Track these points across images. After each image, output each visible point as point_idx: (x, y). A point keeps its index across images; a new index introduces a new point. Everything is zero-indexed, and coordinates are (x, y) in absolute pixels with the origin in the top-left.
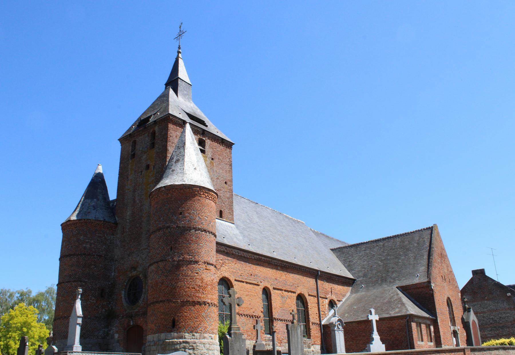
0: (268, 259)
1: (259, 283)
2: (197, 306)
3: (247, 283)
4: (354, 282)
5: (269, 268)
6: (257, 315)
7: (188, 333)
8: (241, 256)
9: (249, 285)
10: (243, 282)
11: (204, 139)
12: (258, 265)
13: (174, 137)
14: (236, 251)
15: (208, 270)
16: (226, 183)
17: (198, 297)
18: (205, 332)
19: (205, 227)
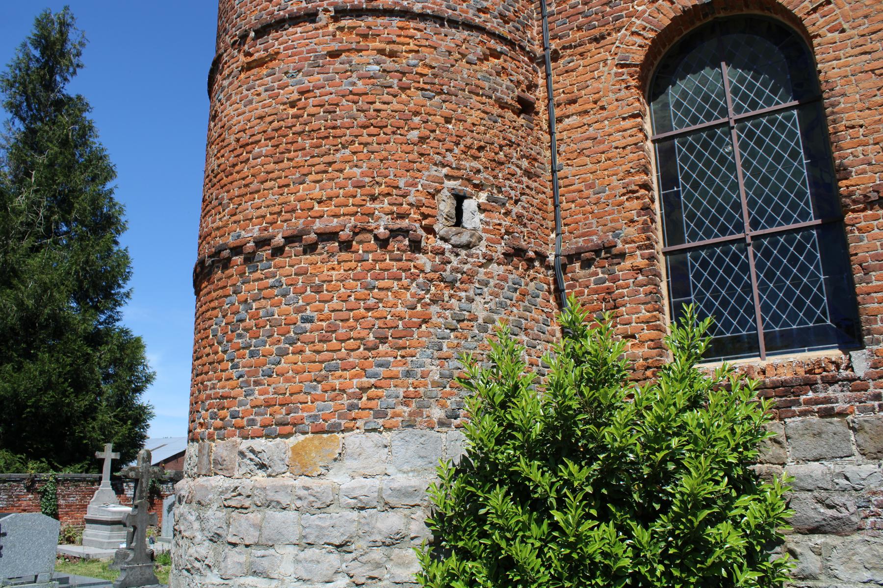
15: (261, 63)
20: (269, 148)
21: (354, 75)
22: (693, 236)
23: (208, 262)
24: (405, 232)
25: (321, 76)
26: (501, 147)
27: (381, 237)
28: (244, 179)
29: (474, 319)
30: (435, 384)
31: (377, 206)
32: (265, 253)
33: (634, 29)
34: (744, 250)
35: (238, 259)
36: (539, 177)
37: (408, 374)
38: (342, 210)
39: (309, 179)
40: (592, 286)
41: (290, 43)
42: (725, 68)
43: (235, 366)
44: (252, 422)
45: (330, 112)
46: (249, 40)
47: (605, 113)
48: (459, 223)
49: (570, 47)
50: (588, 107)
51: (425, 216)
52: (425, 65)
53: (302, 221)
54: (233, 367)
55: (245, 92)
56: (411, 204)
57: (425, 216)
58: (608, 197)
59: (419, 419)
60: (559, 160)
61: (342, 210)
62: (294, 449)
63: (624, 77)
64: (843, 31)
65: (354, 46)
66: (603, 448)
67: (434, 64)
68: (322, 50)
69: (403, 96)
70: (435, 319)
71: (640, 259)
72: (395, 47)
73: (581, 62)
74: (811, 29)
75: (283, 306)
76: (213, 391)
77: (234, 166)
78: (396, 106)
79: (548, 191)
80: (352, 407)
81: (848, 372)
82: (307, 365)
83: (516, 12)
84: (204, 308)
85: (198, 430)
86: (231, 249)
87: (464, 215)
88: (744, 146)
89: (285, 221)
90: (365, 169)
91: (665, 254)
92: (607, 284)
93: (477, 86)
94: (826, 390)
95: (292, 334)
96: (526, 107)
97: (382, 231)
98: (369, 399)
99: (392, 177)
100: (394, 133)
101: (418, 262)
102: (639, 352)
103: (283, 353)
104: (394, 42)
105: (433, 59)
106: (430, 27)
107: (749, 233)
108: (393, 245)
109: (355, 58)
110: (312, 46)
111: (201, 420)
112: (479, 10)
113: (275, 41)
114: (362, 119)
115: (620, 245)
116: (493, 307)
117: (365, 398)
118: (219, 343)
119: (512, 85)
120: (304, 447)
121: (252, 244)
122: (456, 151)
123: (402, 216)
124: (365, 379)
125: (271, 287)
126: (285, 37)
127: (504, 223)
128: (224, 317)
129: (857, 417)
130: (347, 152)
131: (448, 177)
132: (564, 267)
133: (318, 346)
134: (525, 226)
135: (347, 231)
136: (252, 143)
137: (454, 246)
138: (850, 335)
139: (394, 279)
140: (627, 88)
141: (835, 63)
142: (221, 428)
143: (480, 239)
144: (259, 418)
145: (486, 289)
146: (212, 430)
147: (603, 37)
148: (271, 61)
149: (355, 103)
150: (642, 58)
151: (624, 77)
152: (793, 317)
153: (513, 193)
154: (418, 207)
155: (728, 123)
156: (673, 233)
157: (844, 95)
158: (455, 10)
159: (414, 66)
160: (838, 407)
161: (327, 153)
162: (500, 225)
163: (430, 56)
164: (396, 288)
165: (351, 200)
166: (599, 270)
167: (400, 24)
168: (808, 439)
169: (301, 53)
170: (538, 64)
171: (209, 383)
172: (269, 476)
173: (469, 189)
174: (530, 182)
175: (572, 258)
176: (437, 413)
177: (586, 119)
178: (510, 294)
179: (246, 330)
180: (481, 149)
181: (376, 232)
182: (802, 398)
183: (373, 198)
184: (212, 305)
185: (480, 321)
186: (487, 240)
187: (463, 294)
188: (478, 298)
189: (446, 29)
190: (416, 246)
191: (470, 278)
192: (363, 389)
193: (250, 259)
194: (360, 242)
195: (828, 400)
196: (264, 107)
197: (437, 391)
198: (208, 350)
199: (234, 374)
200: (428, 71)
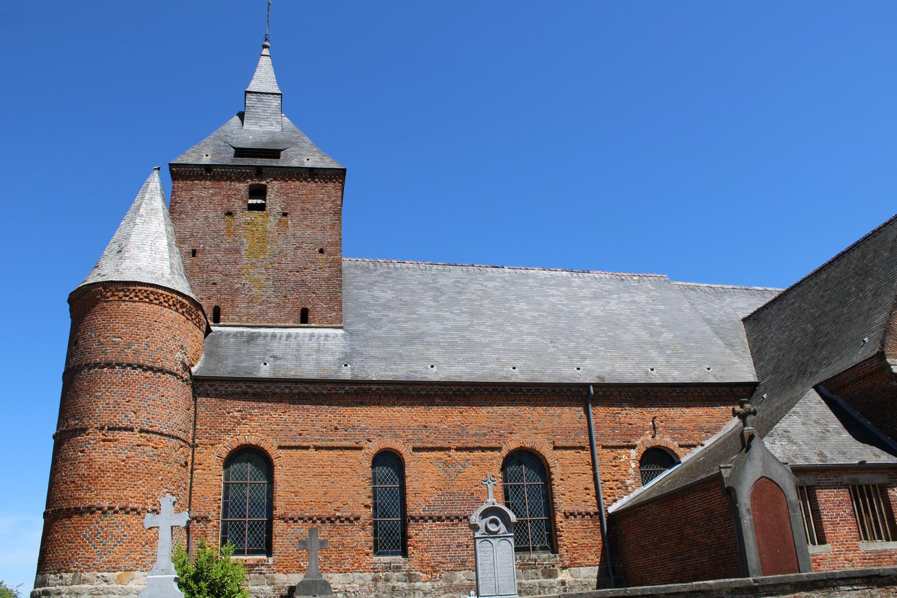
1: (362, 444)
2: (76, 518)
3: (317, 448)
4: (754, 390)
5: (403, 405)
7: (55, 573)
9: (325, 453)
10: (307, 448)
11: (264, 183)
12: (362, 404)
13: (185, 201)
15: (110, 441)
16: (321, 251)
17: (77, 499)
18: (88, 569)
19: (111, 357)
22: (231, 517)
35: (100, 512)
78: (156, 467)
103: (115, 545)
106: (167, 438)
109: (146, 449)
113: (118, 435)
129: (268, 575)
138: (269, 553)
141: (279, 476)
152: (255, 546)
156: (225, 515)
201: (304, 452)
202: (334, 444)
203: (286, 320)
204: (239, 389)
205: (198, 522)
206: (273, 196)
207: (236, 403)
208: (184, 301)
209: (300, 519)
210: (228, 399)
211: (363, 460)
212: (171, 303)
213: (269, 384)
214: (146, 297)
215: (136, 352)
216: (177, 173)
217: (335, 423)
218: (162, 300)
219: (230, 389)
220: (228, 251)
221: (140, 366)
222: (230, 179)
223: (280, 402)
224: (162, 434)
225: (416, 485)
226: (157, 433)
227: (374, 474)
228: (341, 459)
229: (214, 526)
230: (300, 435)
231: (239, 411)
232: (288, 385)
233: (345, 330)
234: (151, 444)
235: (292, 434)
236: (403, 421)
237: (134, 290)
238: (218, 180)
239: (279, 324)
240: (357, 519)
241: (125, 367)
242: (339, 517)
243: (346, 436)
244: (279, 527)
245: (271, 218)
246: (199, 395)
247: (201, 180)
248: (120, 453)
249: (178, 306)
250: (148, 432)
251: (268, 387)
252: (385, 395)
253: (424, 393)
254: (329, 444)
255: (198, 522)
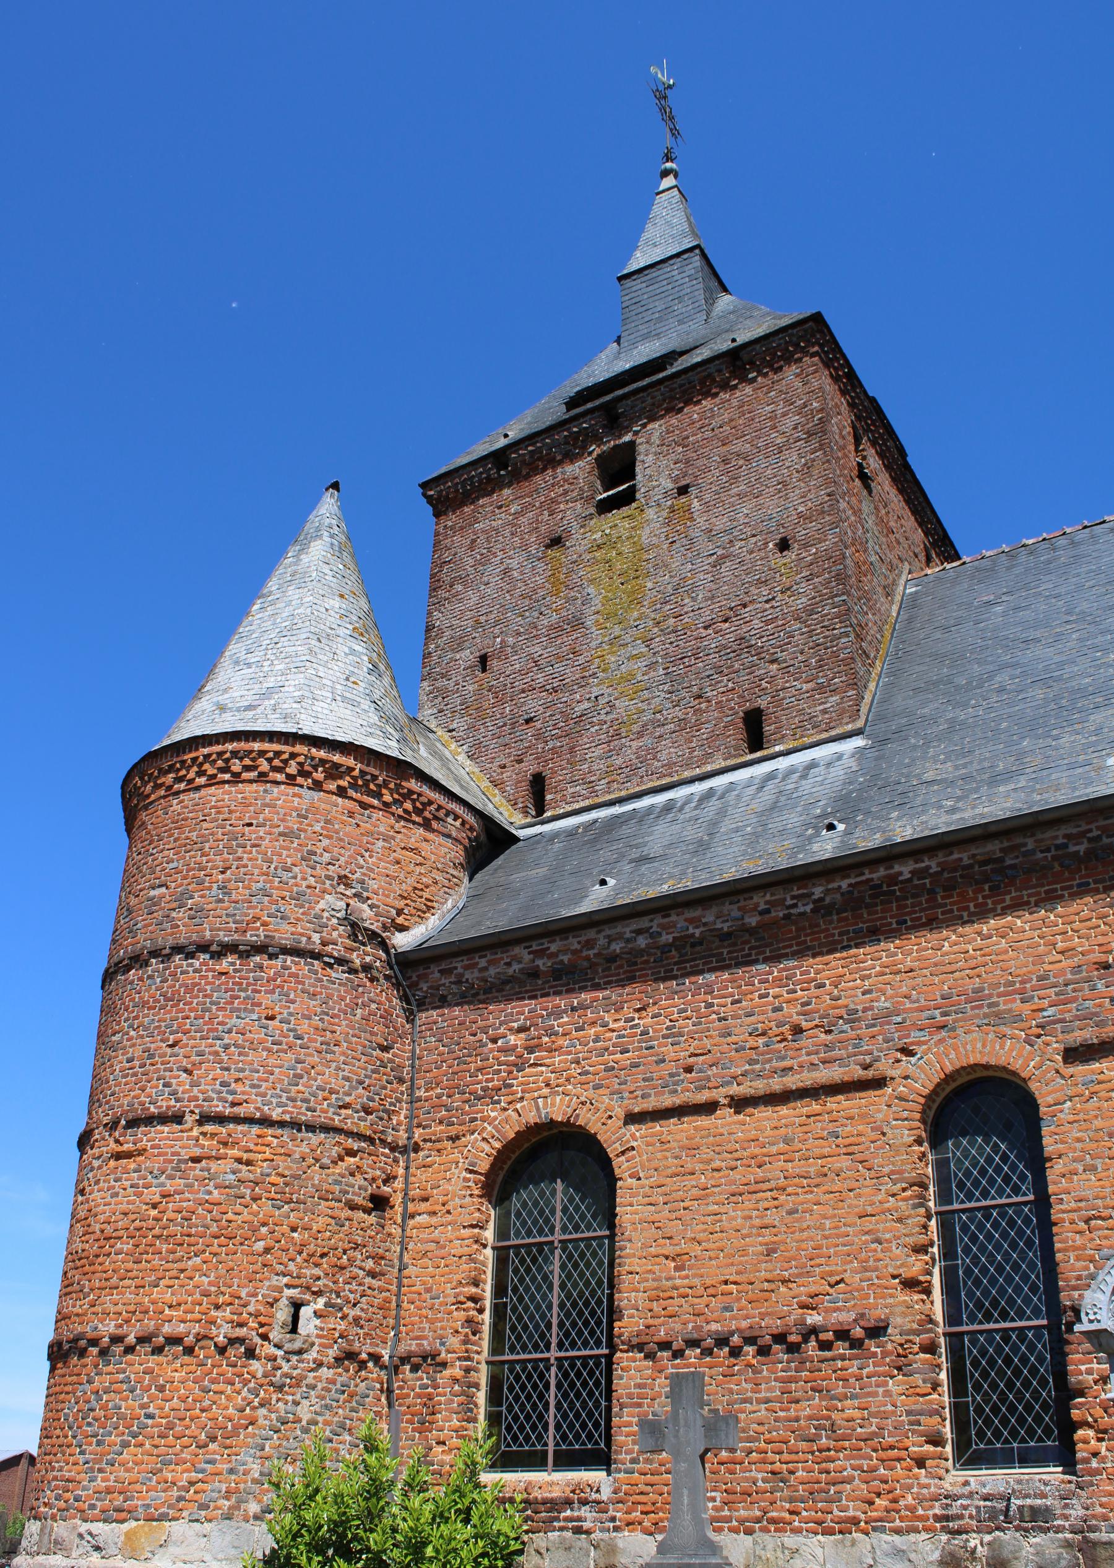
0: (963, 856)
1: (884, 1067)
3: (740, 1104)
5: (1017, 906)
6: (845, 1317)
8: (682, 942)
9: (764, 1114)
10: (710, 1108)
11: (627, 438)
12: (874, 934)
13: (461, 552)
14: (627, 929)
15: (128, 1155)
16: (784, 545)
20: (130, 1246)
21: (212, 1184)
23: (66, 1347)
24: (241, 1340)
25: (182, 1181)
26: (345, 1252)
27: (220, 1345)
28: (105, 1272)
29: (300, 1421)
30: (255, 1481)
31: (220, 1315)
32: (118, 1349)
33: (484, 1135)
34: (548, 1370)
35: (94, 1350)
36: (384, 1275)
37: (231, 1471)
38: (189, 1316)
39: (162, 1283)
40: (417, 1390)
41: (157, 1142)
42: (559, 1185)
43: (82, 1453)
44: (92, 1507)
45: (187, 1220)
46: (119, 1127)
47: (450, 1218)
48: (294, 1330)
49: (430, 1140)
50: (438, 1208)
51: (262, 1325)
52: (278, 1174)
53: (153, 1323)
54: (80, 1453)
55: (113, 1183)
56: (250, 1314)
57: (262, 1325)
58: (441, 1304)
59: (236, 1513)
60: (406, 1258)
61: (189, 1316)
62: (127, 1534)
63: (470, 1184)
64: (639, 1179)
65: (214, 1153)
66: (368, 1550)
67: (287, 1173)
68: (185, 1154)
69: (254, 1206)
70: (261, 1421)
71: (458, 1370)
72: (251, 1156)
73: (437, 1159)
74: (617, 1171)
75: (130, 1401)
76: (59, 1474)
77: (97, 1256)
78: (246, 1215)
79: (394, 1288)
80: (180, 1499)
81: (597, 1495)
82: (146, 1457)
83: (381, 1100)
84: (58, 1389)
85: (42, 1509)
86: (88, 1340)
87: (301, 1322)
88: (563, 1267)
89: (138, 1321)
90: (212, 1278)
91: (487, 1363)
92: (430, 1390)
93: (327, 1191)
94: (580, 1509)
95: (135, 1428)
96: (379, 1203)
97: (221, 1339)
98: (195, 1492)
99: (235, 1287)
100: (242, 1244)
101: (251, 1368)
102: (447, 1458)
103: (125, 1445)
104: (251, 1151)
105: (285, 1168)
106: (286, 1133)
107: (554, 1353)
108: (231, 1351)
109: (214, 1166)
110: (177, 1149)
111: (46, 1500)
112: (340, 1107)
113: (145, 1136)
114: (214, 1229)
115: (443, 1355)
116: (318, 1410)
117: (192, 1491)
118: (70, 1428)
119: (366, 1183)
120: (135, 1533)
121: (107, 1339)
122: (299, 1259)
123: (241, 1325)
124: (193, 1474)
125: (121, 1382)
126: (153, 1134)
127: (339, 1327)
128: (76, 1403)
129: (597, 1535)
130: (198, 1260)
131: (288, 1286)
132: (396, 1368)
133: (157, 1441)
134: (362, 1327)
135: (191, 1337)
136: (115, 1238)
137: (286, 1352)
139: (228, 1383)
140: (471, 1195)
141: (630, 1209)
142: (64, 1510)
143: (313, 1344)
144: (99, 1504)
145: (312, 1393)
146: (55, 1511)
147: (458, 1138)
148: (139, 1155)
149: (210, 1212)
150: (487, 1167)
151: (470, 1184)
153: (352, 1296)
154: (256, 1317)
155: (553, 1242)
157: (630, 1241)
158: (315, 1111)
159: (268, 1175)
160: (586, 1525)
161: (180, 1260)
162: (335, 1329)
163: (282, 1164)
164: (229, 1392)
165: (197, 1307)
166: (425, 1375)
167: (259, 1132)
168: (561, 1552)
169: (166, 1154)
170: (400, 1153)
171: (57, 1465)
172: (103, 1557)
173: (307, 1297)
174: (374, 1281)
175: (404, 1360)
176: (253, 1508)
177: (434, 1220)
178: (337, 1396)
179: (96, 1420)
180: (323, 1255)
181: (216, 1339)
182: (563, 1515)
183: (217, 1307)
184: (66, 1389)
185: (304, 1423)
186: (320, 1345)
187: (290, 1398)
188: (304, 1401)
189: (304, 1134)
190: (251, 1354)
191: (298, 1382)
192: (192, 1483)
193: (104, 1353)
194: (201, 1348)
195: (579, 1519)
196: (128, 1203)
197: (256, 1488)
198: (58, 1431)
199: (82, 1459)
200: (280, 1180)
201: (703, 1121)
202: (792, 1082)
203: (707, 757)
204: (516, 967)
205: (415, 1368)
206: (650, 458)
207: (512, 1007)
208: (337, 758)
209: (693, 1343)
210: (496, 1000)
211: (890, 1125)
212: (292, 769)
213: (591, 934)
214: (223, 770)
215: (198, 912)
216: (438, 499)
217: (792, 1013)
218: (264, 766)
219: (492, 971)
220: (557, 629)
221: (203, 948)
222: (552, 463)
223: (631, 979)
224: (265, 1122)
225: (1086, 1185)
226: (250, 1120)
227: (941, 1166)
228: (817, 1127)
229: (456, 1380)
230: (689, 1070)
231: (521, 1030)
232: (644, 923)
233: (868, 737)
234: (235, 1152)
235: (665, 1070)
236: (1019, 963)
237: (194, 760)
238: (527, 477)
239: (687, 774)
240: (877, 1331)
241: (168, 957)
242: (814, 1331)
243: (828, 1047)
244: (631, 1373)
245: (651, 513)
246: (422, 1005)
247: (490, 494)
248: (147, 1186)
249: (319, 775)
250: (221, 1119)
251: (589, 944)
252: (949, 888)
253: (1082, 848)
254: (776, 1084)
255: (415, 1368)
